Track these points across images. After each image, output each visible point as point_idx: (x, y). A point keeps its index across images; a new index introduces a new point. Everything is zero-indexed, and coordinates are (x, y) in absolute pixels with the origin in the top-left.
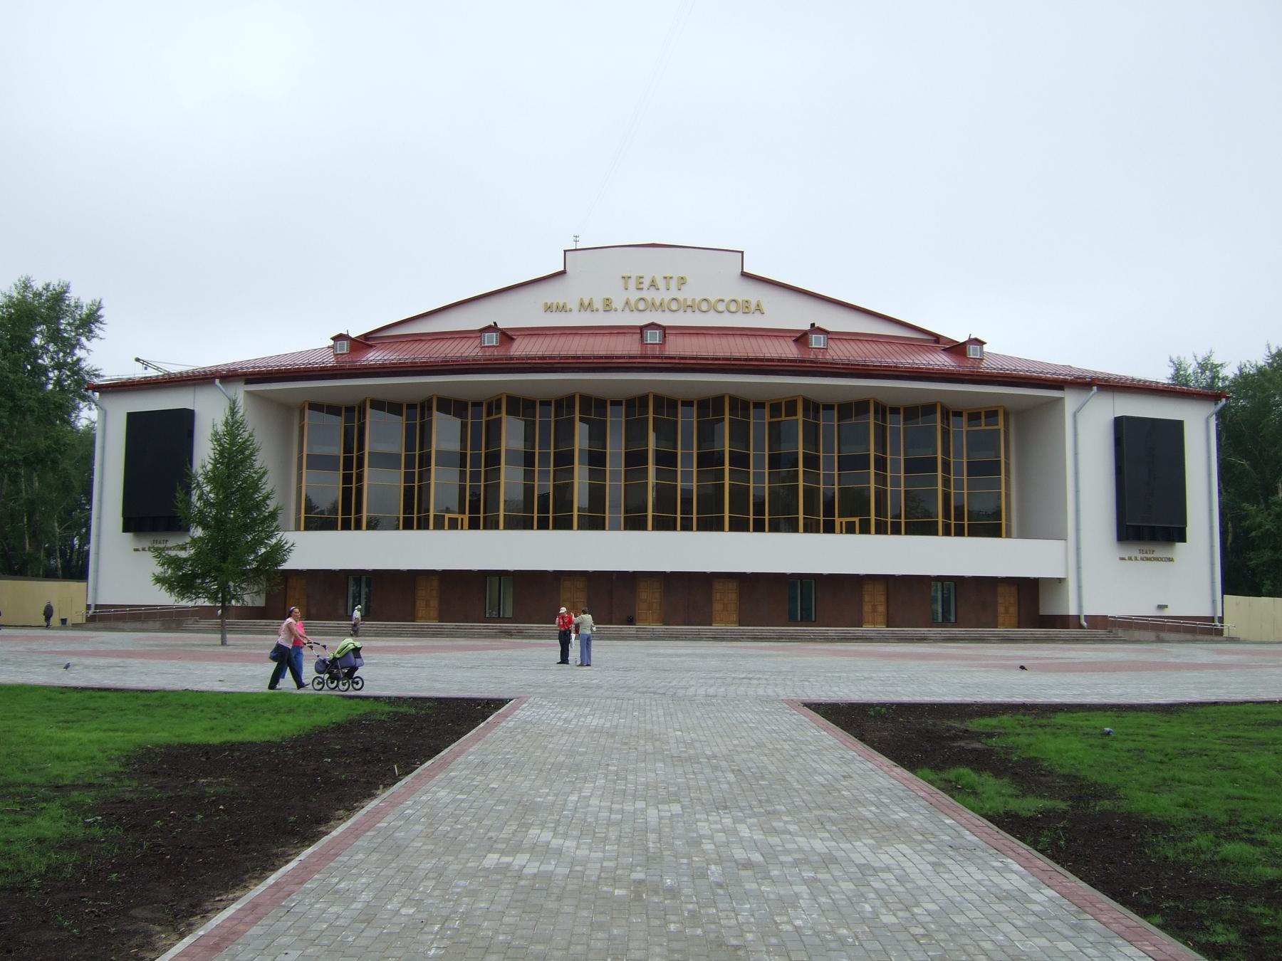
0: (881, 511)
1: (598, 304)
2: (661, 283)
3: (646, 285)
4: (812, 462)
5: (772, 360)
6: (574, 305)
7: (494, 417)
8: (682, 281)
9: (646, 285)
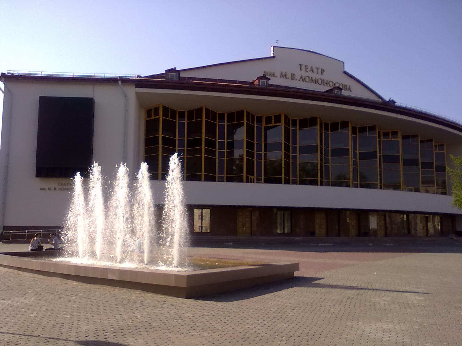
0: (287, 174)
1: (289, 76)
2: (315, 70)
3: (309, 70)
4: (210, 144)
5: (438, 118)
6: (278, 74)
7: (153, 118)
8: (323, 71)
9: (309, 70)
